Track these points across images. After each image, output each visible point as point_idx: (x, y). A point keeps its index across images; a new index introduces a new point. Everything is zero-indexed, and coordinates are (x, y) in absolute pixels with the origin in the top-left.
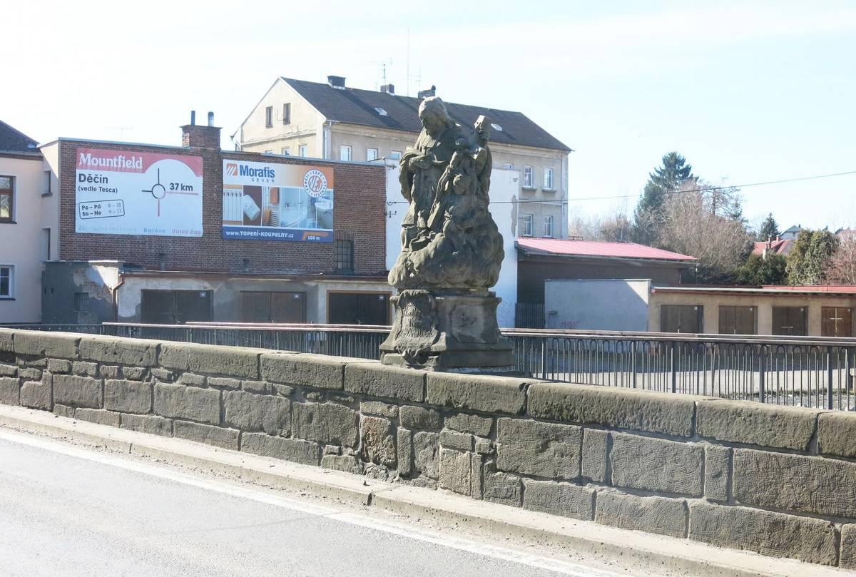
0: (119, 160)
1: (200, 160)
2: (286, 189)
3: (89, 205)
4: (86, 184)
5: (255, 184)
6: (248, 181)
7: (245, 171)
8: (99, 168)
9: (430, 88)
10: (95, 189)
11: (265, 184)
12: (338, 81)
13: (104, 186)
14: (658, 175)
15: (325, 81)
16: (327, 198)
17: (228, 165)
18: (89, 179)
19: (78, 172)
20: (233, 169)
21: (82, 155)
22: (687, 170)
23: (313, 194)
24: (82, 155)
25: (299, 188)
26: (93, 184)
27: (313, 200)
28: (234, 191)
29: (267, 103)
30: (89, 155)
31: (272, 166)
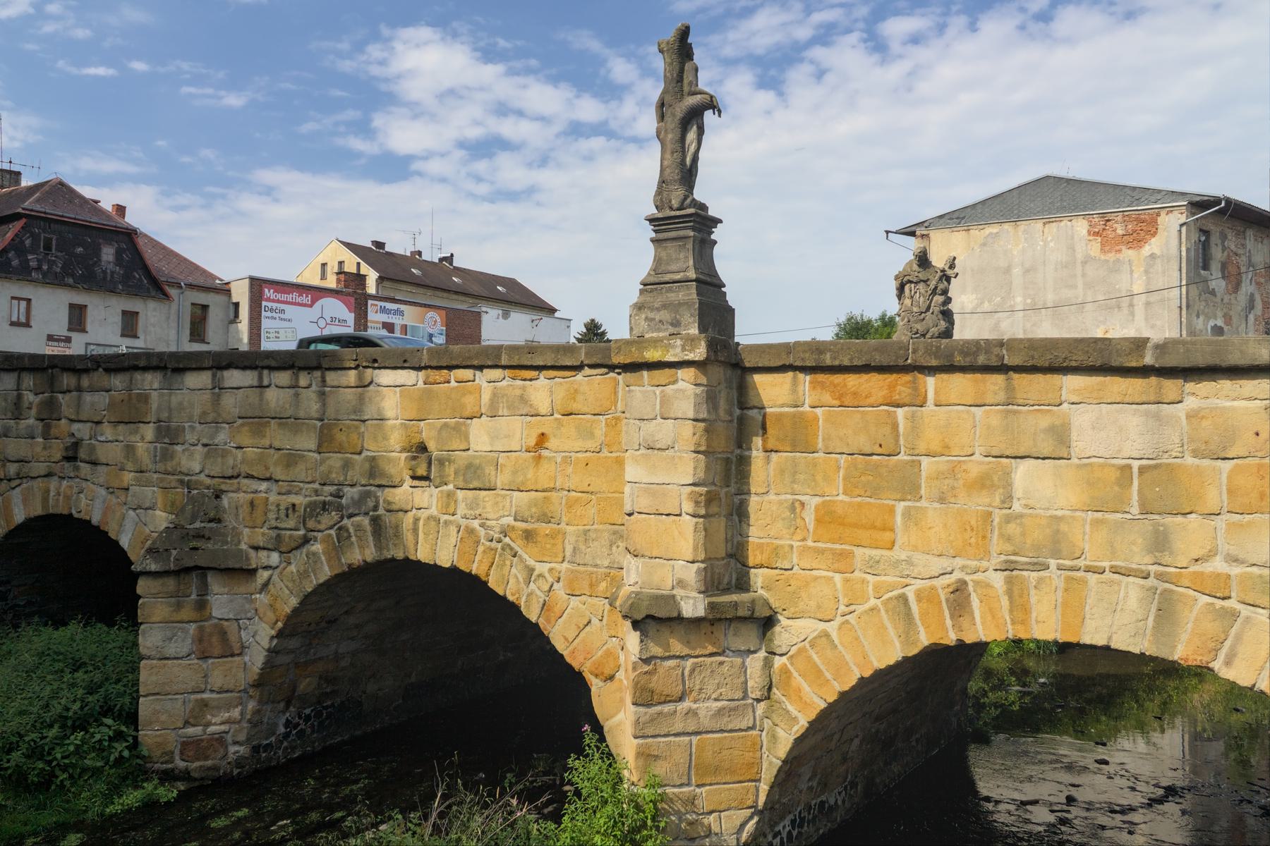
0: (294, 296)
1: (352, 300)
2: (413, 326)
3: (271, 330)
4: (269, 314)
5: (390, 321)
6: (385, 318)
7: (384, 310)
8: (279, 301)
9: (449, 255)
10: (275, 318)
11: (397, 321)
12: (380, 245)
13: (282, 316)
14: (580, 337)
15: (369, 245)
16: (442, 334)
17: (372, 305)
18: (271, 310)
19: (264, 303)
20: (375, 308)
21: (266, 290)
22: (604, 333)
23: (431, 331)
24: (266, 290)
25: (421, 325)
26: (274, 315)
27: (431, 336)
28: (376, 325)
29: (321, 259)
30: (272, 291)
31: (402, 307)
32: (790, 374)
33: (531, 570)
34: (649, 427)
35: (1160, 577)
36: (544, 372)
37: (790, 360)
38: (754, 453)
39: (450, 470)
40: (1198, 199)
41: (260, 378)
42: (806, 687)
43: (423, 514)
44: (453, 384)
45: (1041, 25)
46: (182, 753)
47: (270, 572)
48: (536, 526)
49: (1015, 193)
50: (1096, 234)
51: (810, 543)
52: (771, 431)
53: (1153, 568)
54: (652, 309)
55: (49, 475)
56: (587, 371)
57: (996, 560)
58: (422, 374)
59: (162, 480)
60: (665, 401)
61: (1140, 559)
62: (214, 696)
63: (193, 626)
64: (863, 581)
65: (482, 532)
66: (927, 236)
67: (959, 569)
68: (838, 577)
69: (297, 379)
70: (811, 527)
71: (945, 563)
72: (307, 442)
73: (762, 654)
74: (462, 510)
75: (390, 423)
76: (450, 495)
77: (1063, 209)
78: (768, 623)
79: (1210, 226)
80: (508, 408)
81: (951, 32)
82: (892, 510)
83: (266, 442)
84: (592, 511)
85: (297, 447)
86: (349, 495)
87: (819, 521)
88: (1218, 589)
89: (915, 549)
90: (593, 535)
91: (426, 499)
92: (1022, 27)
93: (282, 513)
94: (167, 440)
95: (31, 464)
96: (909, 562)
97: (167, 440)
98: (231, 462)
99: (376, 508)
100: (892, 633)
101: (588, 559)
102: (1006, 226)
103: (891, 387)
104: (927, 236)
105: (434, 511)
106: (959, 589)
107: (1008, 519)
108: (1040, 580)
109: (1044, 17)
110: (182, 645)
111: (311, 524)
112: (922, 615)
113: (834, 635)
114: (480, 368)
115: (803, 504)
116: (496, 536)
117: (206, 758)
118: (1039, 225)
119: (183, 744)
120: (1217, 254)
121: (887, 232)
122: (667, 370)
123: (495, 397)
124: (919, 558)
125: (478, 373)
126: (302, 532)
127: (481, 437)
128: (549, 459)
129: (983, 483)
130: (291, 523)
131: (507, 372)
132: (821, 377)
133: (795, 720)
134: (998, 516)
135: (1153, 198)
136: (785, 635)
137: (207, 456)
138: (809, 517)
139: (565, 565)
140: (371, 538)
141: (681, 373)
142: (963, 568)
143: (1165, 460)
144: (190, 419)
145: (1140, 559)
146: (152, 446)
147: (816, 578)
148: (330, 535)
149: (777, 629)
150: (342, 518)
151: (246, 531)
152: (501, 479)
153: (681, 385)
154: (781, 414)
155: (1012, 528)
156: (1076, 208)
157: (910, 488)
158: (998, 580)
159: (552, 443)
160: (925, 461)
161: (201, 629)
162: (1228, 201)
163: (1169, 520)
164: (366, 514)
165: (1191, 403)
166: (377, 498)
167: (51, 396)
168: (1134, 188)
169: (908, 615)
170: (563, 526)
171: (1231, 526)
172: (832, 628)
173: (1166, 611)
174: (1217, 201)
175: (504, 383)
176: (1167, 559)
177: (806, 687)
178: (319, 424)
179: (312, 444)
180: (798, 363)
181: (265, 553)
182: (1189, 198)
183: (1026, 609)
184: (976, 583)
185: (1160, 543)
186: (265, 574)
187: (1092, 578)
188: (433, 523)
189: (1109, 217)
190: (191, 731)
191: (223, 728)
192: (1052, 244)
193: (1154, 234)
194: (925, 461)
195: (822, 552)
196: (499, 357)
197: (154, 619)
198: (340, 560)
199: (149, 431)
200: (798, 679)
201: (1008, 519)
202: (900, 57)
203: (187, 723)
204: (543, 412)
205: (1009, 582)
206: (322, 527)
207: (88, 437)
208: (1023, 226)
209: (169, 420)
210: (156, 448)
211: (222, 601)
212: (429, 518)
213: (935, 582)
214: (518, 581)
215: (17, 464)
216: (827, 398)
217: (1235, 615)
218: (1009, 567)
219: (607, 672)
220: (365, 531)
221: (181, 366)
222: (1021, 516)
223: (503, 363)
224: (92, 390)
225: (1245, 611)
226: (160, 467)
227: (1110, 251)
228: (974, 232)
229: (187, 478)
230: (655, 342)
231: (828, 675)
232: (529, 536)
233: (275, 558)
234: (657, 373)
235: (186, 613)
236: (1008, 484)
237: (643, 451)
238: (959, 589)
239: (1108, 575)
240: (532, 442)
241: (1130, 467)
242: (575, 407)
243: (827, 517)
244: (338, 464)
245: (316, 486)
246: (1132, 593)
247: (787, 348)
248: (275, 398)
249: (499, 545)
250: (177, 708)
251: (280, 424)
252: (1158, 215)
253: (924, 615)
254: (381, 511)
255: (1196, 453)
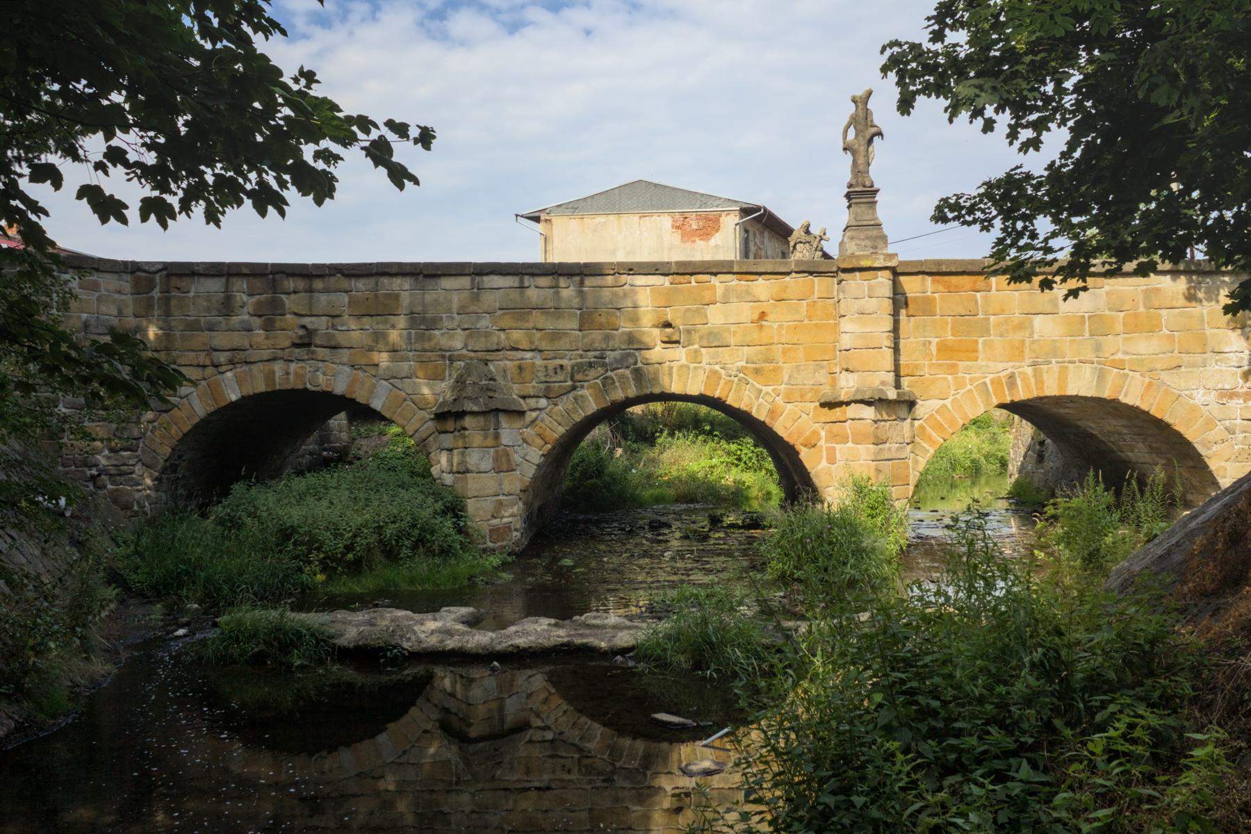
32: (921, 276)
33: (761, 391)
34: (863, 302)
35: (1099, 363)
36: (763, 276)
37: (923, 269)
38: (901, 317)
39: (696, 336)
40: (746, 206)
41: (522, 281)
42: (934, 434)
43: (675, 365)
44: (693, 283)
45: (438, 22)
46: (491, 537)
47: (538, 412)
48: (762, 365)
49: (616, 191)
50: (678, 227)
51: (934, 361)
52: (910, 305)
53: (1096, 359)
54: (859, 239)
55: (274, 359)
56: (794, 275)
57: (1028, 362)
58: (667, 278)
59: (419, 356)
60: (870, 288)
61: (1090, 356)
62: (505, 497)
63: (492, 450)
64: (964, 377)
65: (723, 372)
66: (550, 220)
67: (1010, 367)
68: (950, 377)
69: (558, 282)
70: (935, 353)
71: (1004, 365)
72: (570, 324)
73: (909, 420)
74: (705, 359)
75: (642, 309)
76: (696, 351)
77: (653, 207)
78: (911, 404)
79: (749, 228)
80: (737, 297)
81: (354, 17)
82: (977, 342)
83: (531, 325)
84: (801, 355)
85: (560, 327)
86: (612, 356)
87: (939, 350)
88: (1119, 365)
89: (989, 359)
90: (803, 367)
91: (679, 354)
92: (421, 24)
93: (551, 372)
94: (422, 327)
95: (247, 352)
96: (987, 366)
97: (422, 327)
98: (495, 339)
99: (636, 363)
100: (979, 401)
101: (799, 381)
102: (611, 217)
103: (975, 282)
104: (550, 220)
105: (684, 361)
106: (1012, 377)
107: (1033, 342)
108: (1049, 369)
109: (439, 15)
110: (487, 464)
111: (578, 377)
112: (994, 390)
113: (949, 406)
114: (715, 274)
115: (930, 342)
116: (733, 373)
117: (503, 540)
118: (636, 218)
119: (491, 531)
120: (753, 248)
121: (517, 215)
122: (872, 272)
123: (727, 290)
124: (991, 364)
125: (713, 277)
126: (570, 383)
127: (716, 316)
128: (769, 326)
129: (1020, 327)
130: (560, 377)
131: (735, 276)
132: (937, 278)
133: (928, 451)
134: (1028, 342)
135: (715, 204)
136: (922, 409)
137: (468, 337)
138: (934, 348)
139: (783, 386)
140: (632, 383)
141: (880, 273)
142: (1012, 367)
143: (1099, 313)
144: (449, 310)
145: (1090, 356)
146: (405, 332)
147: (938, 379)
148: (596, 383)
149: (917, 406)
150: (607, 371)
151: (515, 386)
152: (732, 341)
153: (880, 279)
154: (916, 297)
155: (1035, 346)
156: (662, 207)
157: (985, 331)
158: (1029, 370)
159: (770, 317)
160: (992, 318)
161: (497, 451)
162: (765, 210)
163: (1101, 338)
164: (628, 367)
165: (1107, 288)
166: (636, 357)
167: (273, 297)
168: (703, 195)
169: (988, 391)
170: (780, 364)
171: (1124, 339)
172: (948, 402)
173: (1101, 376)
174: (758, 209)
175: (733, 283)
176: (1101, 355)
177: (934, 434)
178: (579, 312)
179: (575, 325)
180: (928, 270)
181: (534, 400)
182: (739, 204)
183: (1042, 382)
184: (1019, 373)
185: (1098, 348)
186: (534, 414)
187: (1071, 366)
188: (685, 369)
189: (686, 215)
190: (495, 522)
191: (510, 519)
192: (646, 233)
193: (717, 230)
194: (992, 318)
195: (941, 365)
196: (732, 267)
197: (475, 445)
198: (605, 398)
199: (402, 322)
200: (929, 430)
201: (1033, 342)
202: (306, 37)
203: (493, 517)
204: (763, 299)
205: (1035, 371)
206: (588, 378)
207: (325, 327)
208: (624, 218)
209: (425, 312)
210: (410, 333)
211: (509, 432)
212: (682, 366)
213: (1001, 374)
214: (750, 398)
215: (228, 353)
216: (941, 288)
217: (1127, 375)
218: (1034, 364)
219: (813, 442)
220: (628, 378)
221: (439, 273)
222: (1039, 340)
223: (735, 270)
224: (326, 291)
225: (1131, 374)
226: (419, 347)
227: (688, 241)
228: (587, 220)
229: (447, 354)
230: (866, 257)
231: (946, 426)
232: (757, 371)
233: (543, 402)
234: (865, 273)
235: (490, 442)
236: (1032, 326)
237: (857, 315)
238: (1012, 377)
239: (1077, 364)
240: (756, 317)
241: (1083, 317)
242: (785, 296)
243: (943, 348)
244: (599, 337)
245: (580, 352)
246: (1087, 370)
247: (921, 263)
248: (533, 295)
249: (736, 379)
250: (488, 505)
251: (542, 313)
252: (720, 216)
253: (994, 390)
254: (639, 365)
255: (1110, 309)
